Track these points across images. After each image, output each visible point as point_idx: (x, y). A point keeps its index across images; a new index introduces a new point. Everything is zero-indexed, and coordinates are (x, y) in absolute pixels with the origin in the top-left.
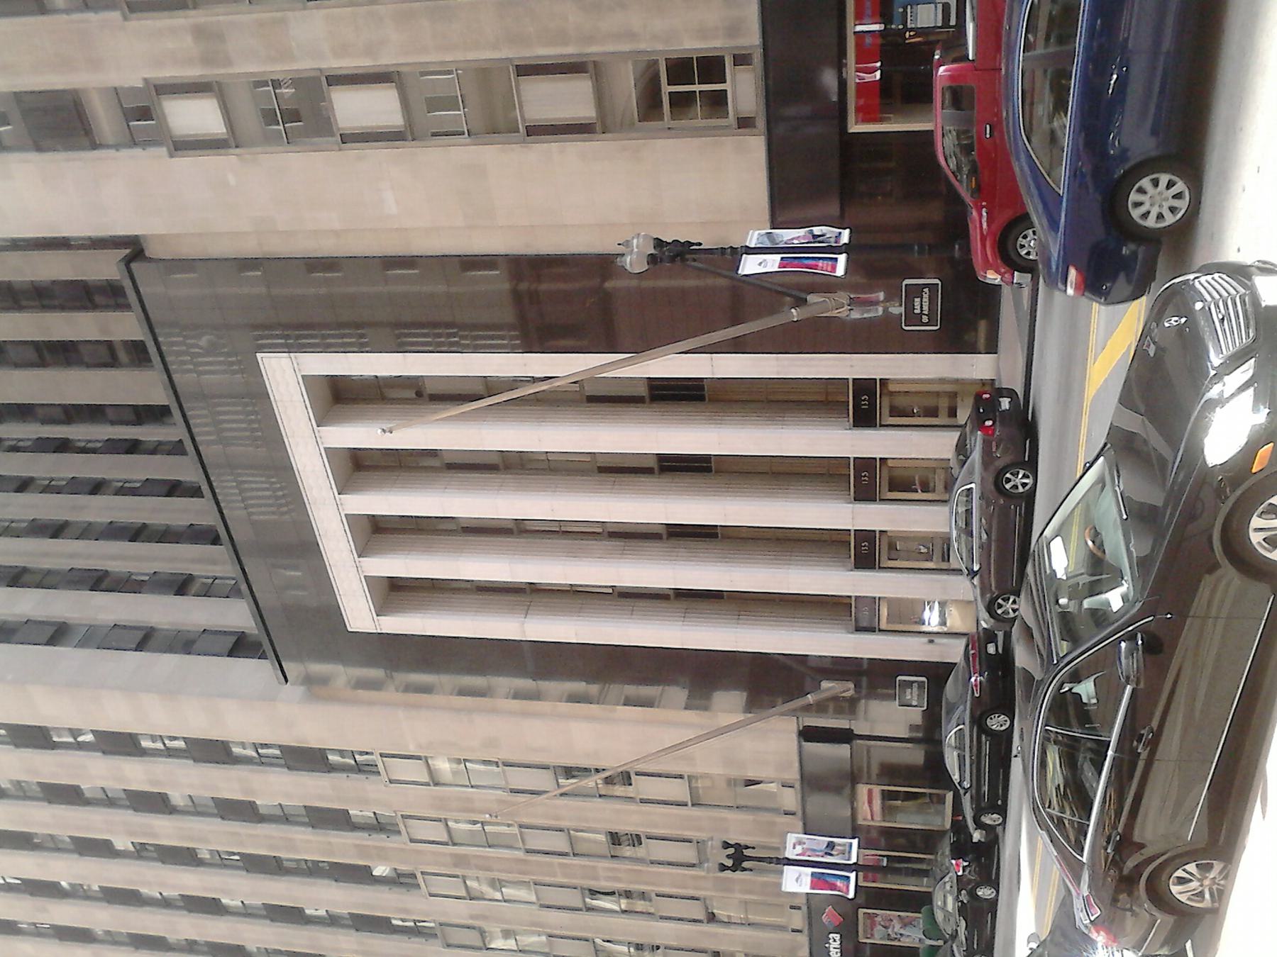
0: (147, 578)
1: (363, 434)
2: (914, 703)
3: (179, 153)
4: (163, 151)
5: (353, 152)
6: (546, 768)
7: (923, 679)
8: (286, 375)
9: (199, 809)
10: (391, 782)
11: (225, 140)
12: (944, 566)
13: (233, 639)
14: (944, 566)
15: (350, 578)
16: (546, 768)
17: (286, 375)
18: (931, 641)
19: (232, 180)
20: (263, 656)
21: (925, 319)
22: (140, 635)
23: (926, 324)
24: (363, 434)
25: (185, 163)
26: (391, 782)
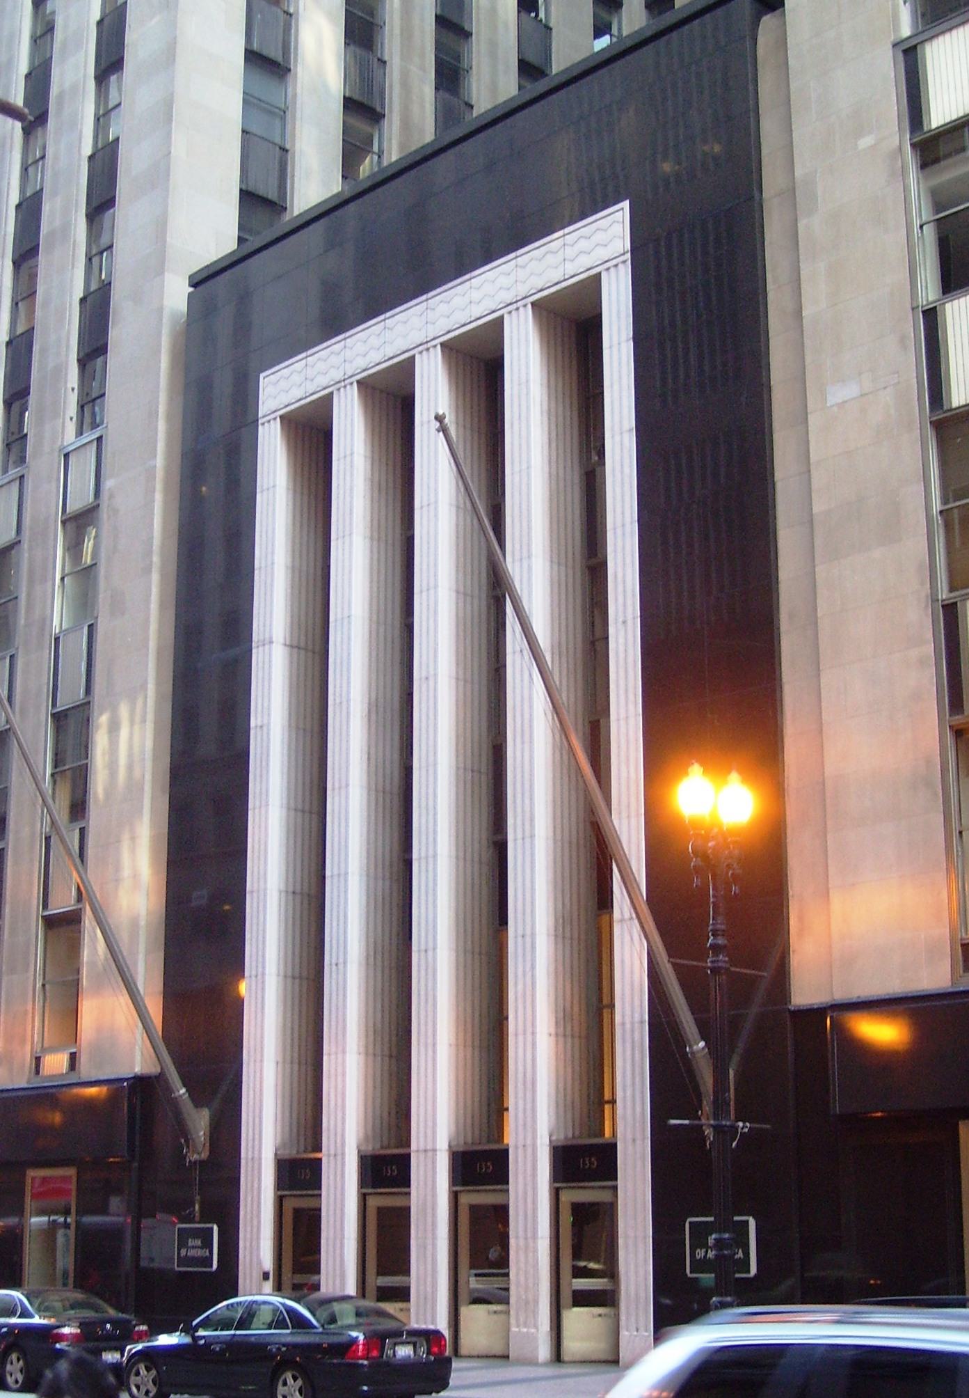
0: (542, 15)
1: (435, 394)
2: (183, 1252)
3: (901, 57)
4: (906, 31)
5: (914, 331)
6: (88, 690)
7: (753, 1270)
8: (598, 247)
9: (31, 170)
10: (66, 456)
11: (921, 123)
12: (566, 1296)
13: (272, 195)
14: (566, 1296)
15: (329, 370)
16: (88, 690)
17: (598, 247)
18: (266, 1276)
19: (866, 142)
20: (241, 240)
21: (700, 1253)
22: (274, 53)
23: (747, 1254)
24: (435, 394)
25: (887, 68)
26: (66, 456)
